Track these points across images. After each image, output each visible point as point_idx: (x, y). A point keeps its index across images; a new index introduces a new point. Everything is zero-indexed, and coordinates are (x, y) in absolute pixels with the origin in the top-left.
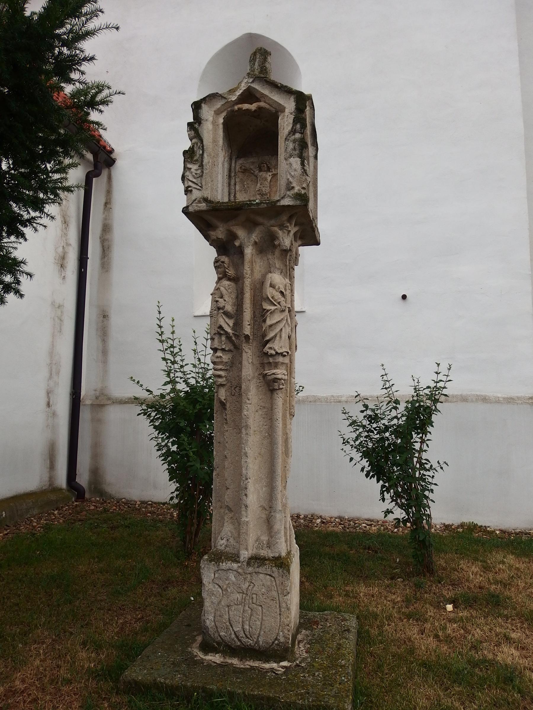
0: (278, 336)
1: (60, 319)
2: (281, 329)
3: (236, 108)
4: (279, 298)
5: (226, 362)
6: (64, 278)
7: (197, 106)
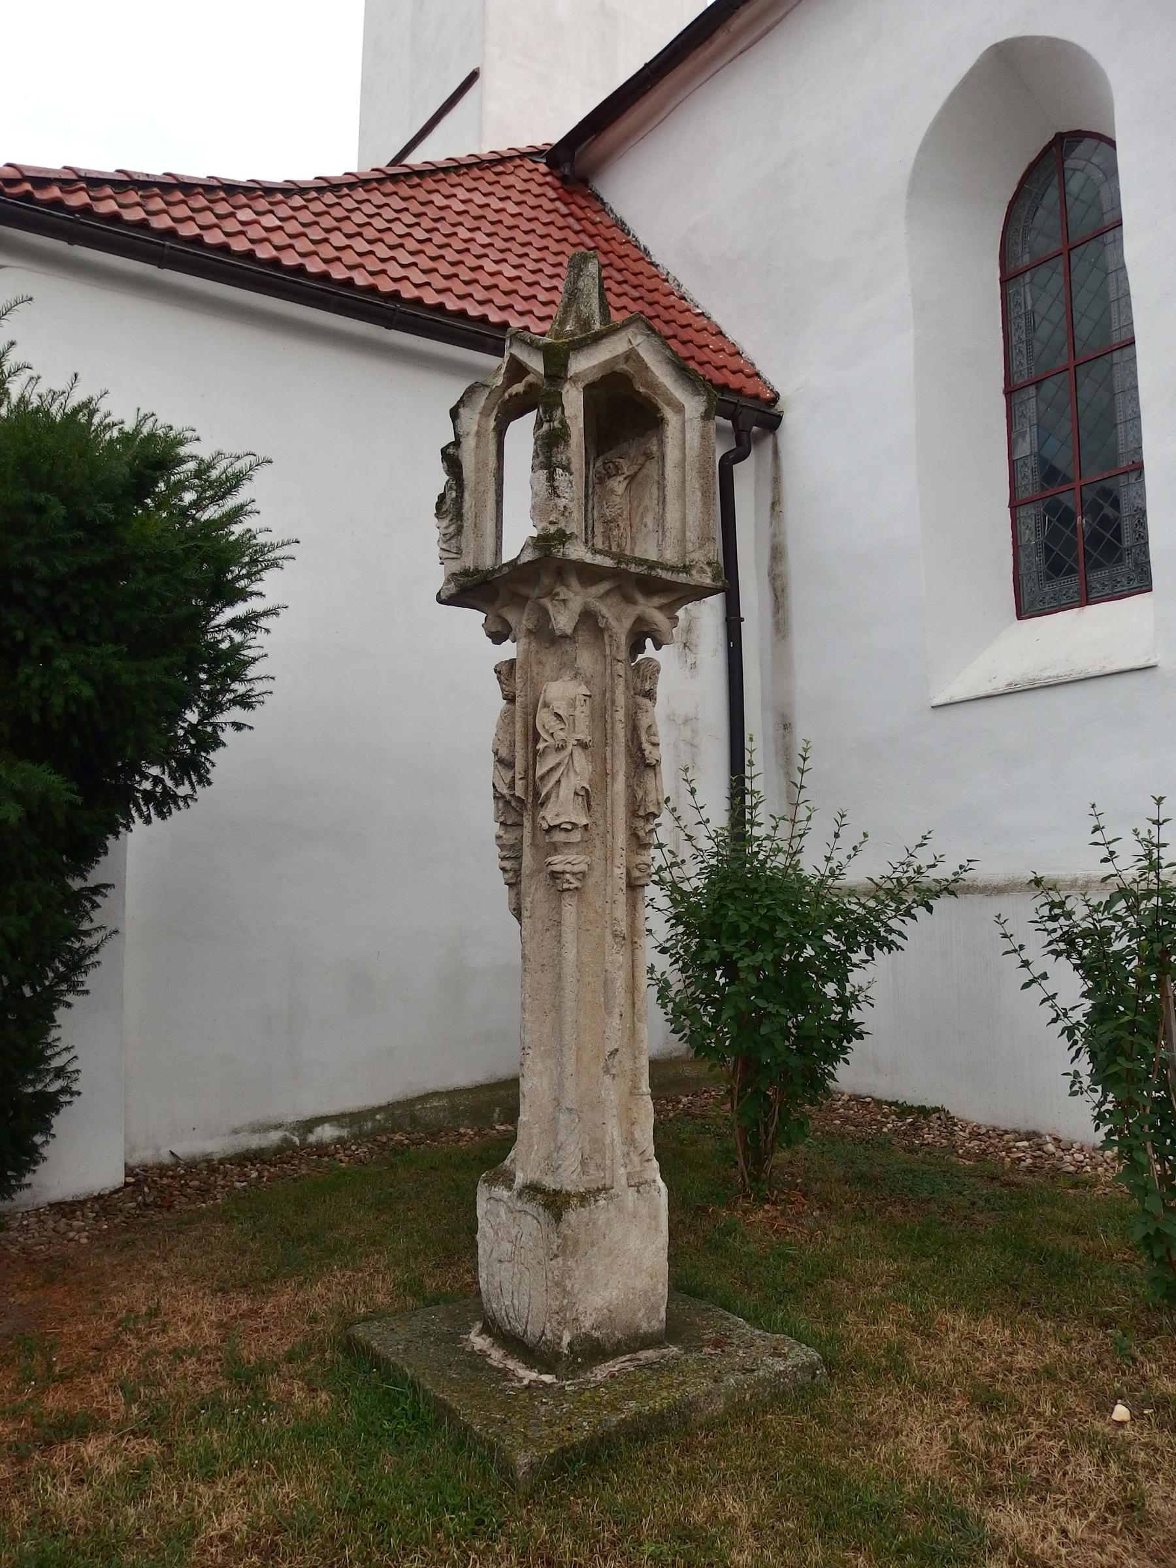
0: (554, 795)
1: (691, 745)
2: (559, 781)
3: (506, 395)
4: (551, 727)
5: (512, 845)
6: (694, 666)
7: (454, 414)
